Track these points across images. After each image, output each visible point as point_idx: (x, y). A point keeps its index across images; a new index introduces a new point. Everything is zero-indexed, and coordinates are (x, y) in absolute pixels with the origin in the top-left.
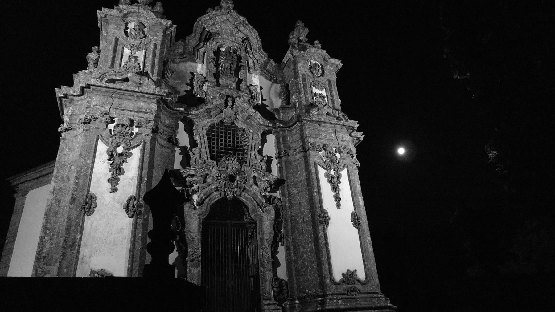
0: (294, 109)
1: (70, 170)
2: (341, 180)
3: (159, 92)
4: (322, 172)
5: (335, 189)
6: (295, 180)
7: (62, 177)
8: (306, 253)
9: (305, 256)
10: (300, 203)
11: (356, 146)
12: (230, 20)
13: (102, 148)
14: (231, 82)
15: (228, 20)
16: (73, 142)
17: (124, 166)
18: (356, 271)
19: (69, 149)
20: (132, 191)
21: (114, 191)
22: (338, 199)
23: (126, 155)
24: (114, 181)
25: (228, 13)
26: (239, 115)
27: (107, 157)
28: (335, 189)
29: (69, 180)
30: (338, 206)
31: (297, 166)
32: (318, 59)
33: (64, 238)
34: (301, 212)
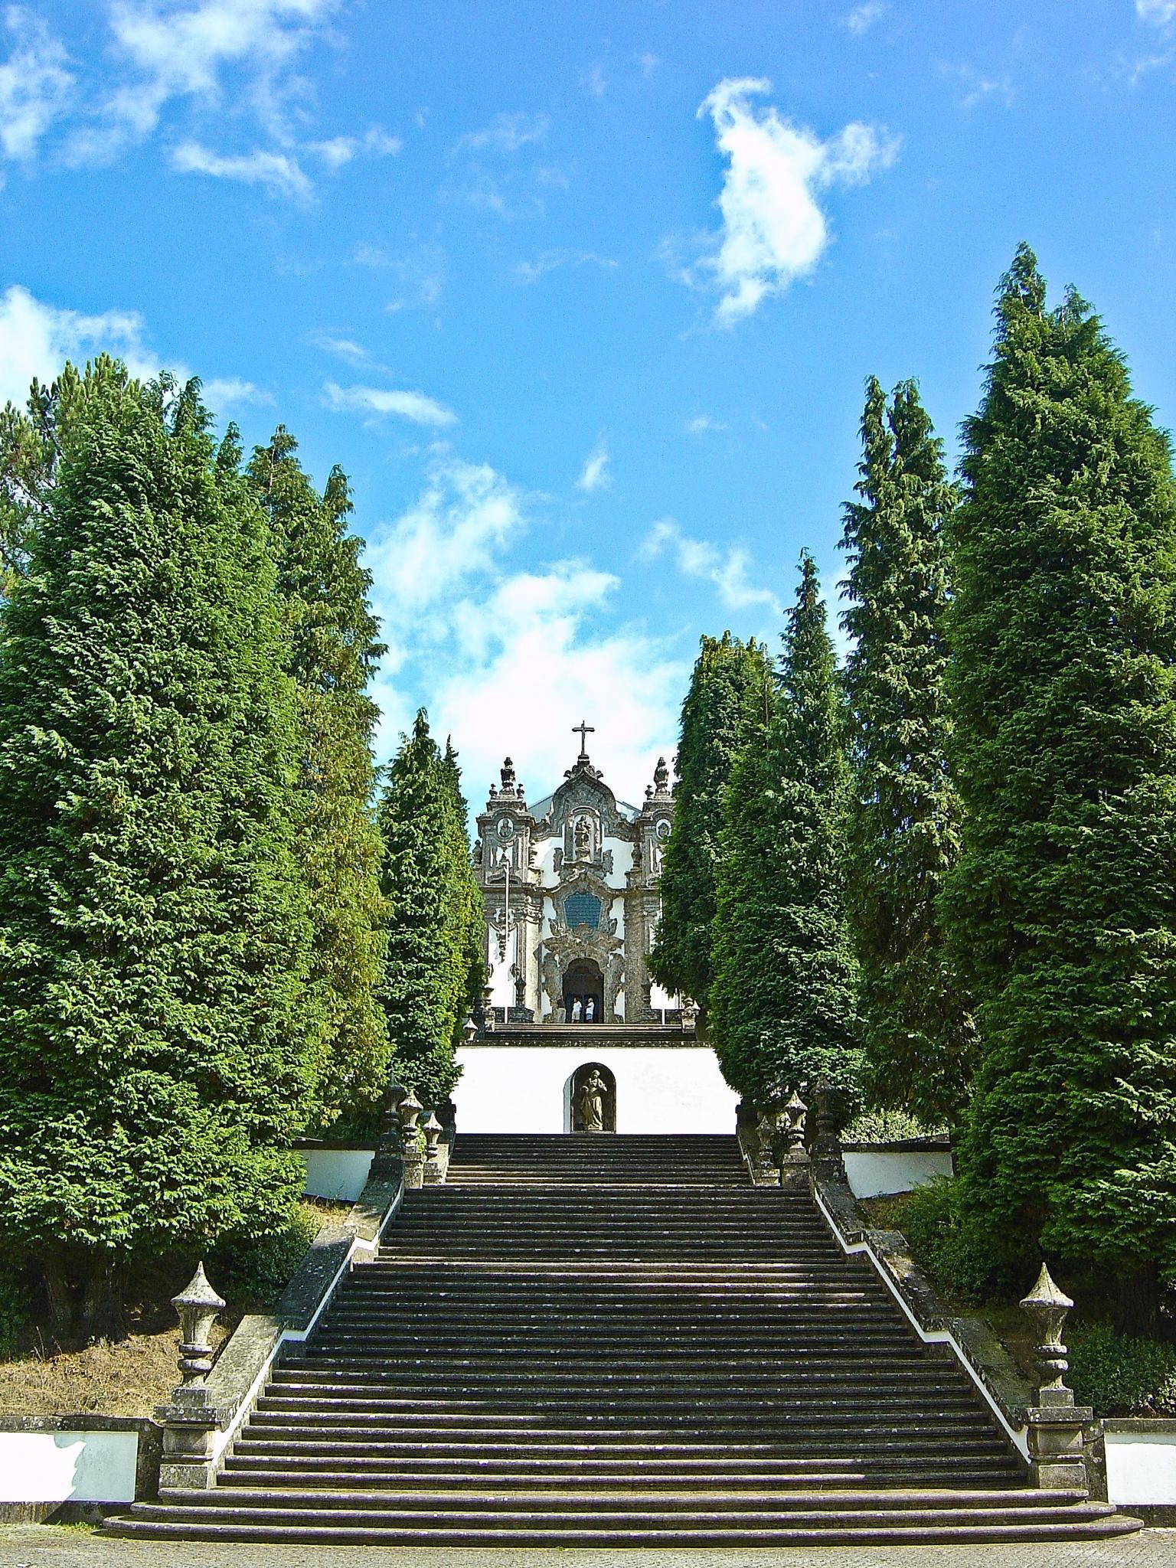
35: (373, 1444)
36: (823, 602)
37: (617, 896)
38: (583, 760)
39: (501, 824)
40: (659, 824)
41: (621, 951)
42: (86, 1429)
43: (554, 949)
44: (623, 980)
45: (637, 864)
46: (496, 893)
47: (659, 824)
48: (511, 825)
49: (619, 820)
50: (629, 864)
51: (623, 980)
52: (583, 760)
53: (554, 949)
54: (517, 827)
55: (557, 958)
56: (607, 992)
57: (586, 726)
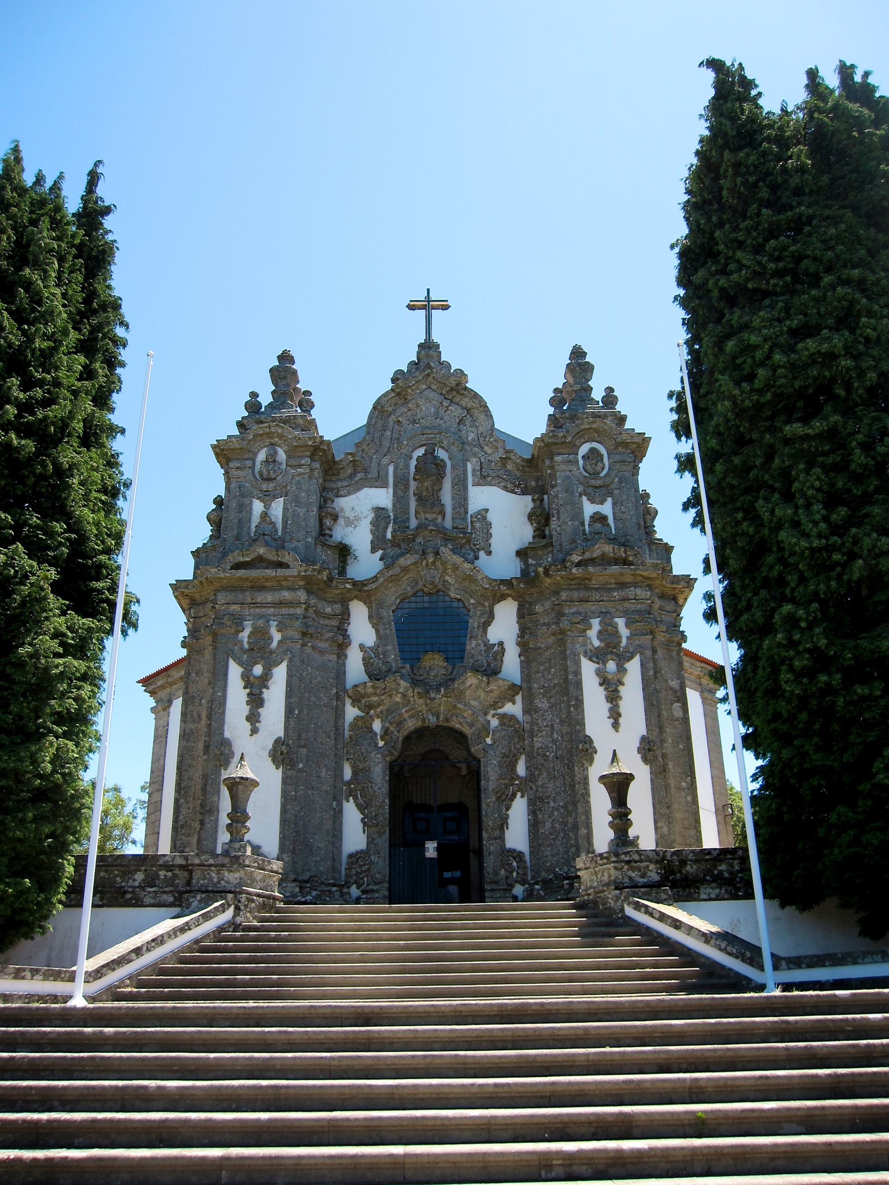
0: (550, 549)
1: (201, 705)
2: (626, 680)
3: (306, 571)
4: (588, 669)
5: (613, 697)
6: (546, 685)
7: (192, 716)
8: (558, 810)
9: (556, 814)
10: (552, 725)
11: (225, 804)
12: (434, 387)
13: (235, 671)
14: (434, 516)
15: (429, 387)
16: (200, 662)
17: (266, 694)
18: (638, 837)
19: (196, 674)
20: (279, 730)
21: (254, 731)
22: (615, 716)
23: (264, 680)
24: (253, 718)
25: (428, 375)
26: (450, 576)
27: (242, 684)
28: (613, 697)
29: (201, 720)
30: (616, 726)
31: (550, 660)
32: (599, 436)
33: (471, 614)
34: (553, 741)
35: (785, 1018)
36: (866, 74)
37: (503, 597)
38: (428, 348)
39: (262, 456)
40: (584, 449)
41: (515, 709)
42: (156, 737)
43: (370, 707)
44: (521, 769)
45: (540, 533)
46: (243, 590)
47: (584, 449)
48: (282, 455)
49: (501, 453)
50: (525, 533)
51: (521, 769)
52: (428, 348)
53: (370, 707)
54: (293, 462)
55: (377, 726)
56: (489, 801)
57: (433, 297)
